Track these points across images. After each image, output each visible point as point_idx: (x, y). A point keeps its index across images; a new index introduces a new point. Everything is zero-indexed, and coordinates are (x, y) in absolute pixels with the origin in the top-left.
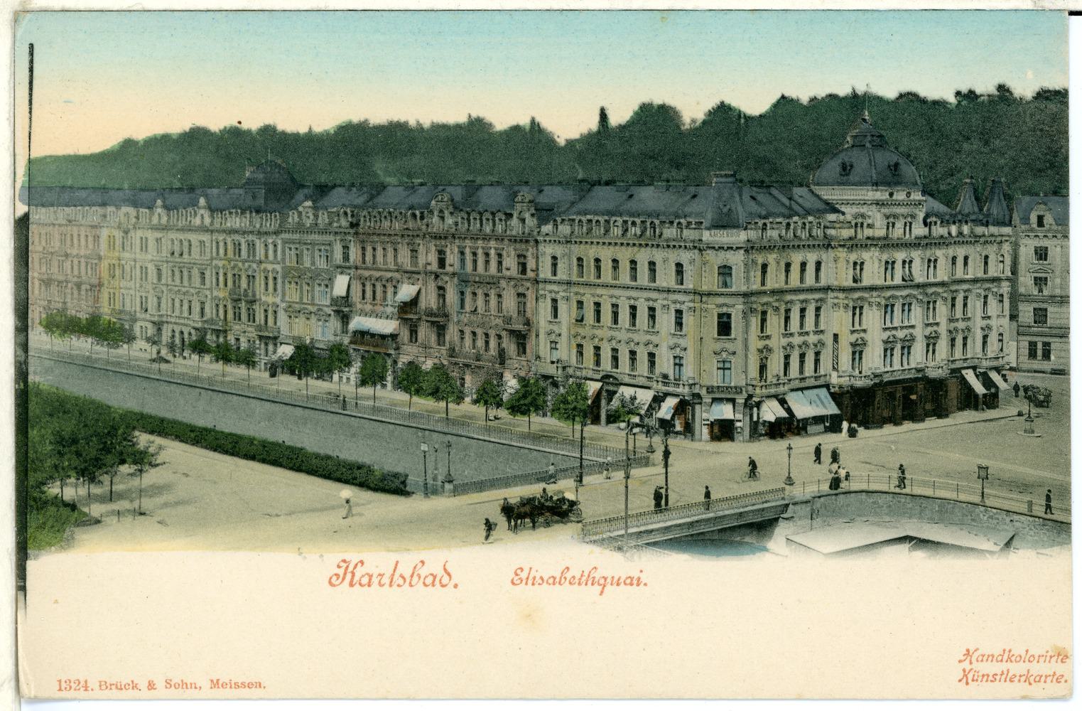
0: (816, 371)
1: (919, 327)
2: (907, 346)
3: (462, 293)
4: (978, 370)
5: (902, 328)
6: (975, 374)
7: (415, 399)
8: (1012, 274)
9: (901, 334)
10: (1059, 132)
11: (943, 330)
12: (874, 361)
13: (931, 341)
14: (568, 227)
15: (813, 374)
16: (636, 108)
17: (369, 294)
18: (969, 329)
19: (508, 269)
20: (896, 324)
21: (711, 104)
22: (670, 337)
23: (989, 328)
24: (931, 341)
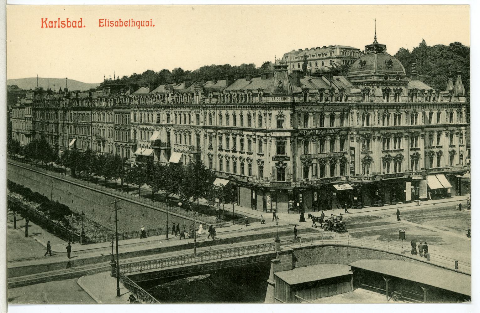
0: (438, 166)
1: (457, 146)
2: (399, 160)
3: (176, 135)
4: (447, 175)
5: (395, 151)
6: (446, 176)
7: (211, 247)
8: (467, 122)
9: (394, 154)
10: (12, 250)
11: (422, 153)
12: (377, 168)
13: (415, 158)
14: (216, 99)
15: (437, 167)
16: (223, 64)
17: (143, 137)
18: (441, 152)
19: (192, 122)
20: (390, 149)
21: (251, 62)
22: (257, 155)
23: (454, 151)
24: (415, 158)
